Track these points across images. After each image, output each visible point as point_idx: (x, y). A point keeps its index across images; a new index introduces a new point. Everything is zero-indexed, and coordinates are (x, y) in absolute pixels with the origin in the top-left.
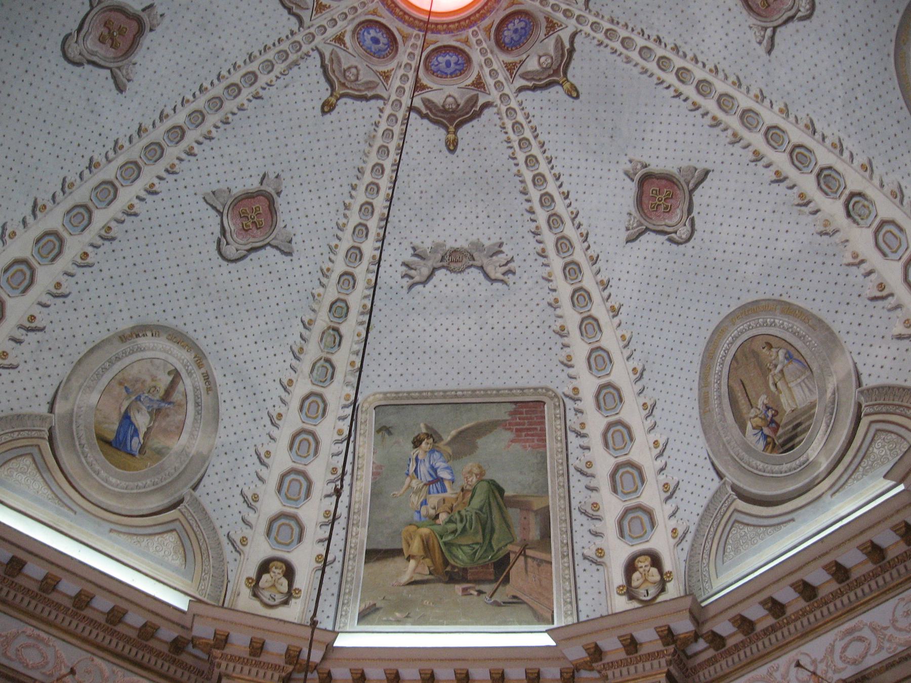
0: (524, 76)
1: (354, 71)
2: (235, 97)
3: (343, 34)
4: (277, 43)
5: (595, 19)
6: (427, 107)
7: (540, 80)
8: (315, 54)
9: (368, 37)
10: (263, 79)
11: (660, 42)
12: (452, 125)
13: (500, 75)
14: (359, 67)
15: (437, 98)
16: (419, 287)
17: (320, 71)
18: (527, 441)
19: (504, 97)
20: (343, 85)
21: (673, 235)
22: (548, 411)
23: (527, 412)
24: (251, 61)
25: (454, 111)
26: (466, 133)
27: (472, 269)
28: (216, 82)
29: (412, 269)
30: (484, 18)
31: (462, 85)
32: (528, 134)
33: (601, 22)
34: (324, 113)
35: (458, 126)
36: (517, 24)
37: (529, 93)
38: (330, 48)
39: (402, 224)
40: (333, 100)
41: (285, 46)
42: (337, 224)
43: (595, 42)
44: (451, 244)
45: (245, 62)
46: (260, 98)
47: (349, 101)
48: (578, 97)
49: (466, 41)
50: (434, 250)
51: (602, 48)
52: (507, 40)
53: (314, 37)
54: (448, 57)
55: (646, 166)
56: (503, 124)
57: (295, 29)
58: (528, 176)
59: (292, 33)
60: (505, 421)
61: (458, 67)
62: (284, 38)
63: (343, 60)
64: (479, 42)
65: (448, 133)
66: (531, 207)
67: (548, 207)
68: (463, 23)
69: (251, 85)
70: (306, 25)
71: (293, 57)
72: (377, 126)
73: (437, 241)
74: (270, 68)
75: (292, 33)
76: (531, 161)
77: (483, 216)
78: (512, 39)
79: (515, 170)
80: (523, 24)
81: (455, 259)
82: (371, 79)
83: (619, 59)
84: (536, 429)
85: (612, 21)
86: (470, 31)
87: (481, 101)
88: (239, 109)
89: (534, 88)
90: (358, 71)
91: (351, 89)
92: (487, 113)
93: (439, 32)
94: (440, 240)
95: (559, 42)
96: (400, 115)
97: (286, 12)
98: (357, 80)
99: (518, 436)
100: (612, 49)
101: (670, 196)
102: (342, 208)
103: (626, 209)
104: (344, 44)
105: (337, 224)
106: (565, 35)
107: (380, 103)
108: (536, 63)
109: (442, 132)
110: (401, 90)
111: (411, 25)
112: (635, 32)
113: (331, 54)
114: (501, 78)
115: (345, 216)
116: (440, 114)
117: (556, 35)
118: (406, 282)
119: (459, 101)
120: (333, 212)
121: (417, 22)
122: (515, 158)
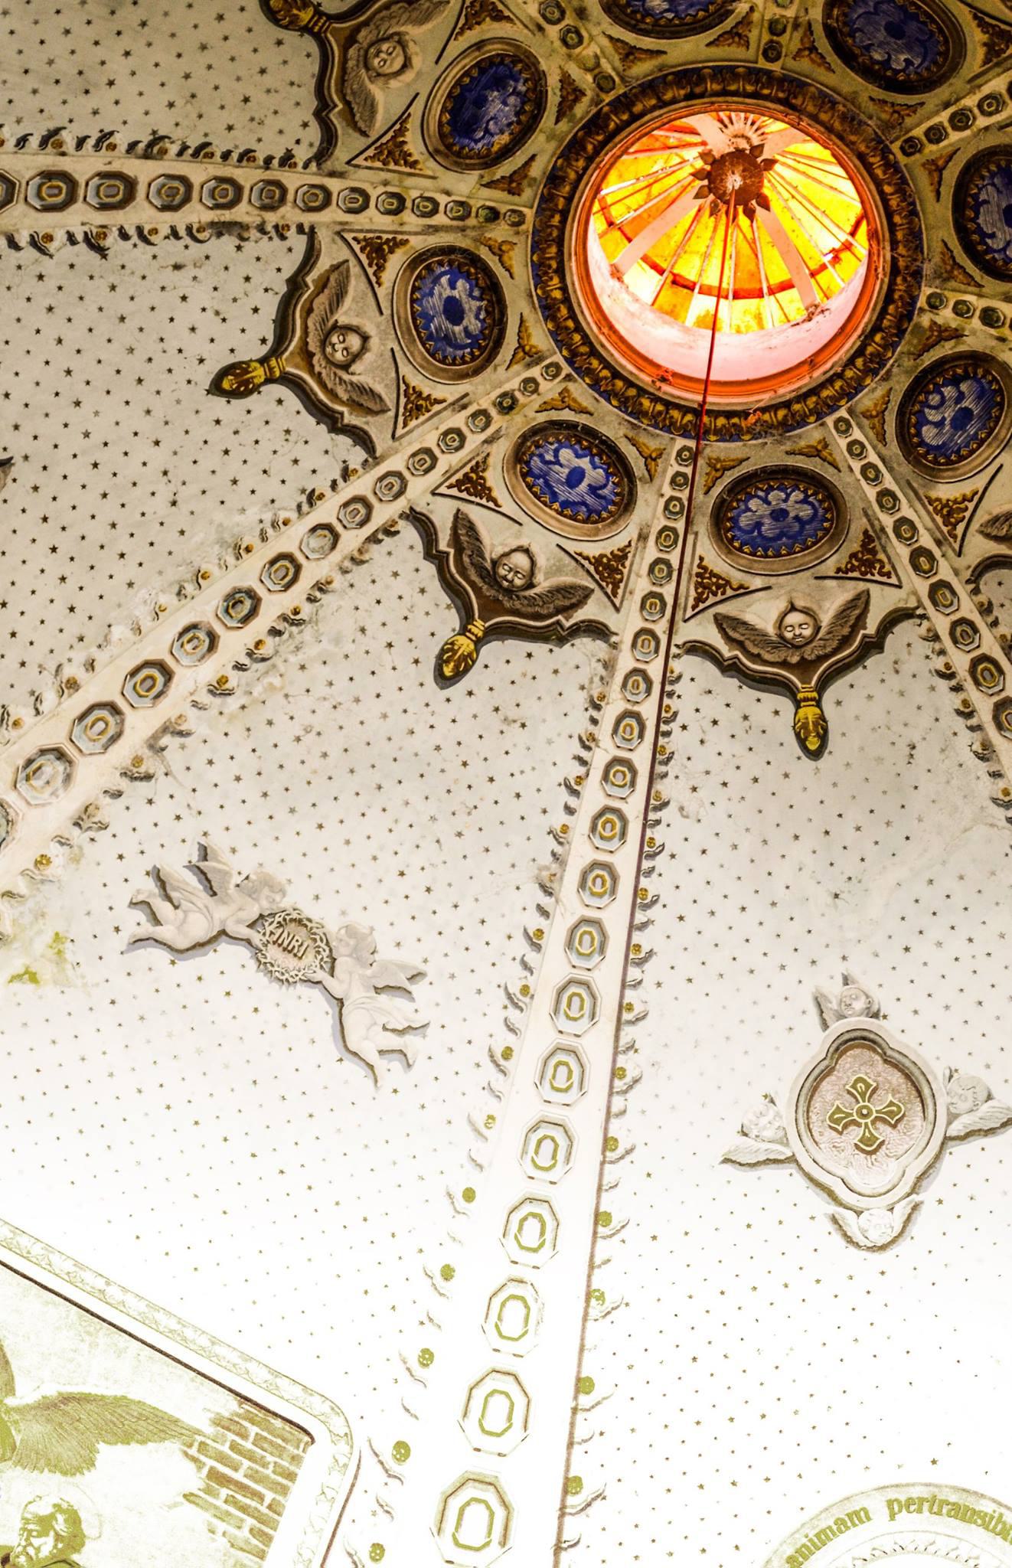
1: (354, 342)
2: (48, 209)
4: (235, 156)
7: (757, 658)
8: (299, 243)
10: (141, 213)
12: (484, 619)
14: (374, 342)
15: (495, 536)
16: (162, 956)
18: (223, 1516)
21: (850, 1215)
22: (316, 1466)
23: (258, 1440)
24: (147, 155)
25: (510, 592)
26: (503, 658)
27: (316, 993)
28: (34, 142)
29: (169, 899)
31: (572, 547)
34: (216, 388)
36: (795, 503)
39: (213, 774)
40: (259, 373)
41: (248, 176)
43: (939, 663)
44: (297, 899)
45: (132, 146)
46: (102, 252)
47: (293, 401)
48: (816, 755)
50: (249, 887)
51: (943, 685)
52: (744, 521)
53: (327, 203)
54: (585, 463)
55: (876, 1015)
57: (302, 154)
59: (287, 160)
60: (198, 1432)
61: (590, 500)
62: (261, 157)
63: (348, 301)
65: (464, 631)
69: (104, 207)
70: (328, 165)
71: (243, 212)
73: (267, 869)
75: (287, 160)
78: (758, 525)
79: (559, 818)
80: (806, 512)
81: (285, 938)
82: (379, 388)
83: (966, 737)
84: (261, 1498)
88: (34, 243)
89: (729, 668)
90: (364, 348)
92: (586, 647)
93: (607, 395)
94: (280, 874)
95: (860, 604)
96: (382, 514)
98: (345, 367)
99: (208, 1491)
100: (965, 703)
101: (893, 1118)
104: (381, 268)
106: (882, 601)
107: (356, 456)
108: (774, 616)
109: (453, 620)
110: (426, 459)
113: (335, 268)
116: (474, 577)
118: (135, 923)
119: (539, 578)
120: (70, 636)
121: (577, 337)
122: (575, 793)
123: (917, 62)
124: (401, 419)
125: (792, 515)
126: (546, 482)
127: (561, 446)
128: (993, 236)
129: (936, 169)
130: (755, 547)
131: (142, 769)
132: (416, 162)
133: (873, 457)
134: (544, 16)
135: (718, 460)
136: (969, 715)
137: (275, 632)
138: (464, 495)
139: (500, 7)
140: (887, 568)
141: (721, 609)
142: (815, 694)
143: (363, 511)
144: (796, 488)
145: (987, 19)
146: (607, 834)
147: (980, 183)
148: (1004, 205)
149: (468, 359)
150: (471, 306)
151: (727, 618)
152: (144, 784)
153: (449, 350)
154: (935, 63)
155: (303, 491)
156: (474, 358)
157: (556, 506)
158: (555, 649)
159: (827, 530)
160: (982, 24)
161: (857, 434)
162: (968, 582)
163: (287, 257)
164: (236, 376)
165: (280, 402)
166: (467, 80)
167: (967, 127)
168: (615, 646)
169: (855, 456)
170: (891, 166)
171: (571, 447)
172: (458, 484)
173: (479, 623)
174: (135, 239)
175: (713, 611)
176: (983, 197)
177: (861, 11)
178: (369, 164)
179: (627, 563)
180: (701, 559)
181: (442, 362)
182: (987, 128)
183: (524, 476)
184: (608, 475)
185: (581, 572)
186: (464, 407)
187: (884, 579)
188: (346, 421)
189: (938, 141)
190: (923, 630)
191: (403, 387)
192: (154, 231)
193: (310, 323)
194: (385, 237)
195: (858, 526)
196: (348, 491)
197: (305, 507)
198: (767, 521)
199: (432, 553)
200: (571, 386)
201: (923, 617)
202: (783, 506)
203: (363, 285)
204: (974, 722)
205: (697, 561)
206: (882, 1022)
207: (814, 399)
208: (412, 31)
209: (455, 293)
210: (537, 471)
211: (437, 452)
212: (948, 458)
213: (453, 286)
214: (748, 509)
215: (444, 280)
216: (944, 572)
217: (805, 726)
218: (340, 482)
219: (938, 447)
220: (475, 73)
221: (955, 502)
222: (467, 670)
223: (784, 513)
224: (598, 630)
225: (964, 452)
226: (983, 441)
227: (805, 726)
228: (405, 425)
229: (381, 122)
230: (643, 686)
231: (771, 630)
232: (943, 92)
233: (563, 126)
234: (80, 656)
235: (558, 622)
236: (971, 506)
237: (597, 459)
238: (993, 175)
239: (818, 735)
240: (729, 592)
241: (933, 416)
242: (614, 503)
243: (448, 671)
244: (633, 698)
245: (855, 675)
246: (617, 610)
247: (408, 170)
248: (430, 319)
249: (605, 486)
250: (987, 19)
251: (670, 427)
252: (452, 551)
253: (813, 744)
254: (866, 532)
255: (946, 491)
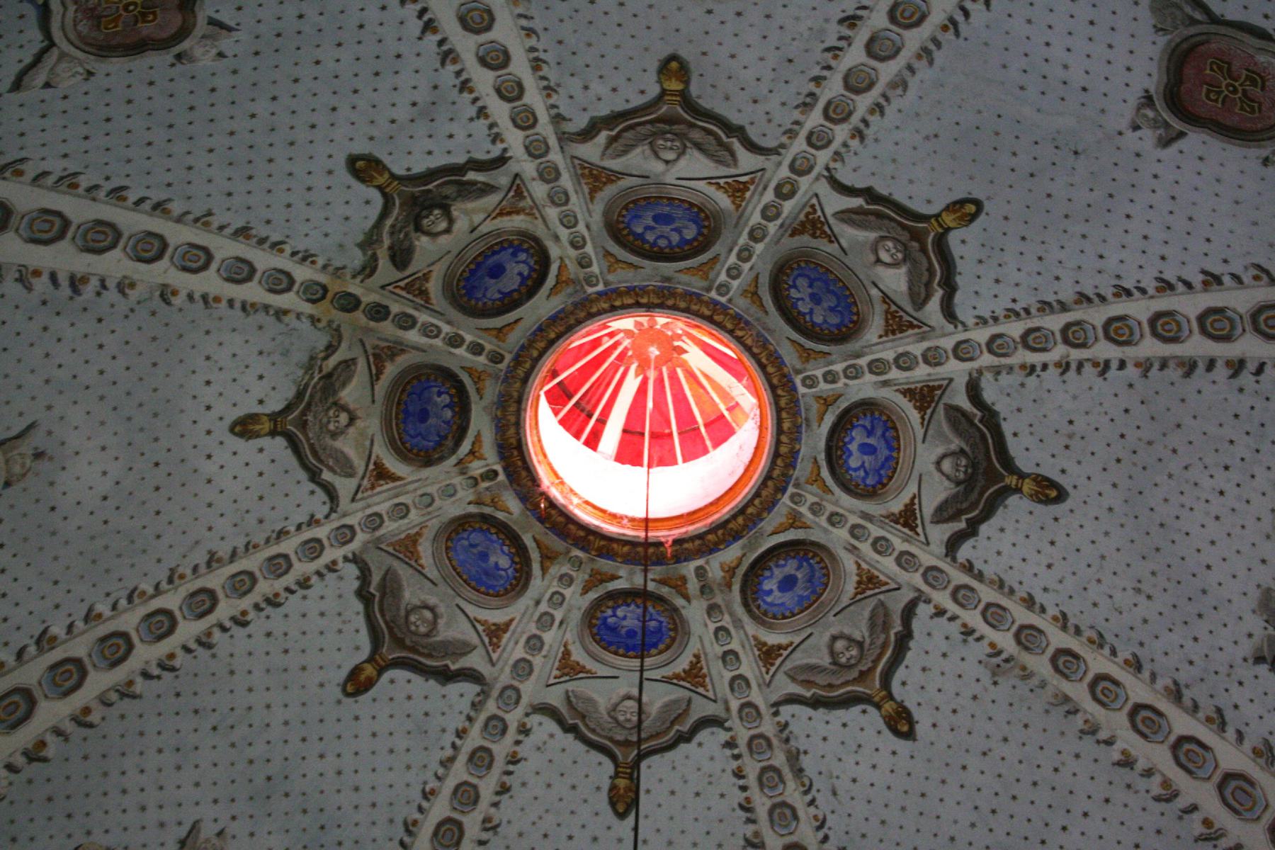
0: (920, 303)
1: (840, 645)
3: (760, 644)
4: (741, 782)
5: (326, 558)
6: (954, 517)
8: (786, 711)
9: (777, 597)
11: (854, 17)
12: (1002, 478)
13: (909, 348)
14: (834, 631)
15: (936, 492)
17: (821, 713)
19: (961, 352)
20: (863, 676)
25: (973, 464)
26: (1027, 453)
30: (779, 357)
31: (920, 432)
32: (1054, 323)
33: (808, 125)
34: (909, 735)
35: (1008, 463)
36: (800, 293)
37: (958, 298)
38: (781, 678)
40: (888, 707)
41: (752, 769)
42: (1158, 799)
43: (855, 143)
47: (900, 674)
48: (978, 204)
49: (827, 402)
51: (869, 132)
52: (834, 320)
53: (749, 704)
54: (853, 447)
56: (1023, 367)
57: (724, 736)
58: (1150, 347)
59: (730, 744)
61: (879, 432)
62: (735, 764)
63: (813, 661)
64: (830, 377)
65: (1018, 490)
66: (1229, 363)
67: (1233, 328)
68: (783, 402)
70: (723, 715)
71: (779, 760)
72: (972, 632)
73: (1254, 605)
74: (788, 812)
75: (730, 744)
76: (1117, 331)
77: (1221, 480)
78: (832, 309)
79: (1131, 372)
80: (802, 282)
82: (867, 614)
83: (896, 103)
85: (806, 106)
86: (802, 390)
87: (963, 402)
89: (950, 288)
91: (876, 661)
92: (989, 394)
93: (794, 454)
94: (1255, 594)
97: (683, 747)
98: (860, 644)
100: (872, 112)
101: (1224, 64)
102: (1124, 775)
103: (1254, 166)
104: (780, 647)
105: (1158, 799)
106: (834, 203)
107: (923, 610)
108: (891, 271)
109: (1013, 500)
110: (905, 560)
111: (770, 505)
112: (833, 63)
113: (793, 679)
114: (917, 349)
115: (1148, 773)
116: (974, 496)
117: (832, 221)
119: (953, 447)
121: (711, 537)
122: (1107, 364)
123: (435, 390)
124: (883, 588)
125: (810, 291)
126: (882, 466)
127: (849, 468)
128: (520, 274)
129: (500, 332)
130: (849, 306)
131: (1215, 716)
132: (695, 656)
133: (733, 259)
134: (552, 625)
135: (801, 356)
136: (878, 105)
137: (1078, 631)
138: (919, 522)
139: (560, 655)
140: (808, 209)
141: (909, 309)
142: (933, 220)
143: (962, 592)
144: (788, 297)
145: (374, 371)
146: (1127, 331)
147: (490, 303)
148: (493, 281)
149: (818, 559)
150: (779, 573)
151: (914, 302)
152: (1225, 713)
153: (817, 574)
154: (428, 379)
155: (965, 641)
156: (815, 555)
157: (895, 454)
158: (1002, 416)
159: (806, 262)
160: (380, 372)
161: (723, 277)
162: (779, 154)
163: (800, 718)
164: (896, 723)
165: (904, 683)
166: (621, 651)
167: (457, 335)
168: (980, 372)
169: (740, 267)
170: (518, 360)
171: (846, 462)
172: (913, 529)
173: (1008, 481)
174: (825, 830)
175: (915, 314)
176: (498, 296)
177: (425, 443)
178: (710, 687)
179: (913, 386)
180: (881, 337)
181: (828, 575)
182: (449, 323)
183: (884, 485)
184: (853, 427)
185: (935, 416)
186: (855, 548)
187: (817, 207)
188: (900, 628)
189: (479, 344)
190: (838, 165)
191: (859, 597)
192: (815, 817)
193: (839, 682)
194: (757, 653)
195: (792, 244)
196: (952, 608)
197: (977, 635)
198: (825, 305)
199: (971, 531)
200: (802, 480)
201: (828, 169)
202: (808, 299)
203: (797, 654)
204: (882, 101)
205: (884, 339)
206: (1152, 91)
207: (716, 318)
208: (603, 704)
209: (775, 587)
210: (877, 478)
211: (896, 554)
212: (698, 213)
213: (771, 592)
214: (825, 321)
215: (769, 599)
216: (784, 172)
217: (961, 218)
218: (948, 615)
219: (695, 222)
220: (613, 648)
221: (726, 192)
222: (1047, 479)
223: (812, 296)
224: (973, 390)
225: (686, 206)
226: (669, 199)
227: (961, 218)
228: (887, 584)
229: (676, 693)
230: (999, 341)
231: (903, 270)
232: (446, 362)
233: (621, 573)
234: (1141, 784)
235: (981, 421)
236: (722, 181)
237: (847, 440)
238: (478, 299)
239: (962, 207)
240: (894, 308)
241: (675, 238)
242: (872, 414)
243: (1054, 494)
244: (1012, 344)
245: (900, 197)
246: (951, 380)
247: (703, 658)
248: (801, 597)
249: (864, 427)
250: (374, 371)
251: (794, 401)
252: (964, 517)
253: (971, 208)
254: (792, 235)
255: (724, 201)
